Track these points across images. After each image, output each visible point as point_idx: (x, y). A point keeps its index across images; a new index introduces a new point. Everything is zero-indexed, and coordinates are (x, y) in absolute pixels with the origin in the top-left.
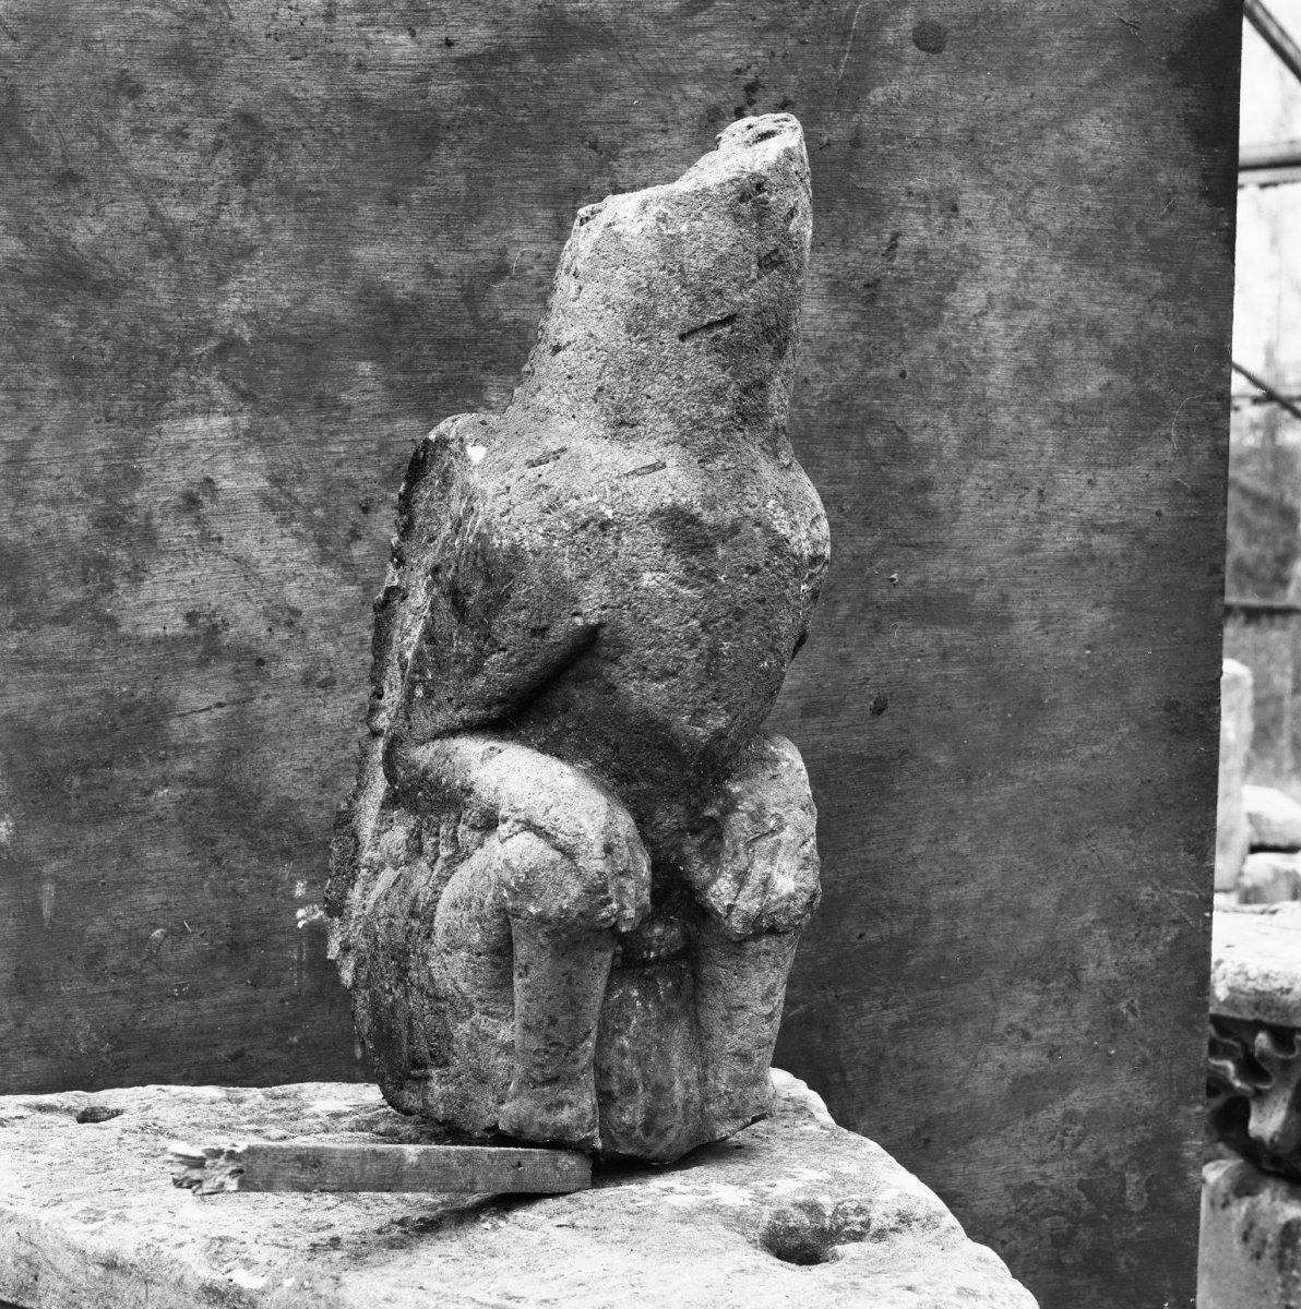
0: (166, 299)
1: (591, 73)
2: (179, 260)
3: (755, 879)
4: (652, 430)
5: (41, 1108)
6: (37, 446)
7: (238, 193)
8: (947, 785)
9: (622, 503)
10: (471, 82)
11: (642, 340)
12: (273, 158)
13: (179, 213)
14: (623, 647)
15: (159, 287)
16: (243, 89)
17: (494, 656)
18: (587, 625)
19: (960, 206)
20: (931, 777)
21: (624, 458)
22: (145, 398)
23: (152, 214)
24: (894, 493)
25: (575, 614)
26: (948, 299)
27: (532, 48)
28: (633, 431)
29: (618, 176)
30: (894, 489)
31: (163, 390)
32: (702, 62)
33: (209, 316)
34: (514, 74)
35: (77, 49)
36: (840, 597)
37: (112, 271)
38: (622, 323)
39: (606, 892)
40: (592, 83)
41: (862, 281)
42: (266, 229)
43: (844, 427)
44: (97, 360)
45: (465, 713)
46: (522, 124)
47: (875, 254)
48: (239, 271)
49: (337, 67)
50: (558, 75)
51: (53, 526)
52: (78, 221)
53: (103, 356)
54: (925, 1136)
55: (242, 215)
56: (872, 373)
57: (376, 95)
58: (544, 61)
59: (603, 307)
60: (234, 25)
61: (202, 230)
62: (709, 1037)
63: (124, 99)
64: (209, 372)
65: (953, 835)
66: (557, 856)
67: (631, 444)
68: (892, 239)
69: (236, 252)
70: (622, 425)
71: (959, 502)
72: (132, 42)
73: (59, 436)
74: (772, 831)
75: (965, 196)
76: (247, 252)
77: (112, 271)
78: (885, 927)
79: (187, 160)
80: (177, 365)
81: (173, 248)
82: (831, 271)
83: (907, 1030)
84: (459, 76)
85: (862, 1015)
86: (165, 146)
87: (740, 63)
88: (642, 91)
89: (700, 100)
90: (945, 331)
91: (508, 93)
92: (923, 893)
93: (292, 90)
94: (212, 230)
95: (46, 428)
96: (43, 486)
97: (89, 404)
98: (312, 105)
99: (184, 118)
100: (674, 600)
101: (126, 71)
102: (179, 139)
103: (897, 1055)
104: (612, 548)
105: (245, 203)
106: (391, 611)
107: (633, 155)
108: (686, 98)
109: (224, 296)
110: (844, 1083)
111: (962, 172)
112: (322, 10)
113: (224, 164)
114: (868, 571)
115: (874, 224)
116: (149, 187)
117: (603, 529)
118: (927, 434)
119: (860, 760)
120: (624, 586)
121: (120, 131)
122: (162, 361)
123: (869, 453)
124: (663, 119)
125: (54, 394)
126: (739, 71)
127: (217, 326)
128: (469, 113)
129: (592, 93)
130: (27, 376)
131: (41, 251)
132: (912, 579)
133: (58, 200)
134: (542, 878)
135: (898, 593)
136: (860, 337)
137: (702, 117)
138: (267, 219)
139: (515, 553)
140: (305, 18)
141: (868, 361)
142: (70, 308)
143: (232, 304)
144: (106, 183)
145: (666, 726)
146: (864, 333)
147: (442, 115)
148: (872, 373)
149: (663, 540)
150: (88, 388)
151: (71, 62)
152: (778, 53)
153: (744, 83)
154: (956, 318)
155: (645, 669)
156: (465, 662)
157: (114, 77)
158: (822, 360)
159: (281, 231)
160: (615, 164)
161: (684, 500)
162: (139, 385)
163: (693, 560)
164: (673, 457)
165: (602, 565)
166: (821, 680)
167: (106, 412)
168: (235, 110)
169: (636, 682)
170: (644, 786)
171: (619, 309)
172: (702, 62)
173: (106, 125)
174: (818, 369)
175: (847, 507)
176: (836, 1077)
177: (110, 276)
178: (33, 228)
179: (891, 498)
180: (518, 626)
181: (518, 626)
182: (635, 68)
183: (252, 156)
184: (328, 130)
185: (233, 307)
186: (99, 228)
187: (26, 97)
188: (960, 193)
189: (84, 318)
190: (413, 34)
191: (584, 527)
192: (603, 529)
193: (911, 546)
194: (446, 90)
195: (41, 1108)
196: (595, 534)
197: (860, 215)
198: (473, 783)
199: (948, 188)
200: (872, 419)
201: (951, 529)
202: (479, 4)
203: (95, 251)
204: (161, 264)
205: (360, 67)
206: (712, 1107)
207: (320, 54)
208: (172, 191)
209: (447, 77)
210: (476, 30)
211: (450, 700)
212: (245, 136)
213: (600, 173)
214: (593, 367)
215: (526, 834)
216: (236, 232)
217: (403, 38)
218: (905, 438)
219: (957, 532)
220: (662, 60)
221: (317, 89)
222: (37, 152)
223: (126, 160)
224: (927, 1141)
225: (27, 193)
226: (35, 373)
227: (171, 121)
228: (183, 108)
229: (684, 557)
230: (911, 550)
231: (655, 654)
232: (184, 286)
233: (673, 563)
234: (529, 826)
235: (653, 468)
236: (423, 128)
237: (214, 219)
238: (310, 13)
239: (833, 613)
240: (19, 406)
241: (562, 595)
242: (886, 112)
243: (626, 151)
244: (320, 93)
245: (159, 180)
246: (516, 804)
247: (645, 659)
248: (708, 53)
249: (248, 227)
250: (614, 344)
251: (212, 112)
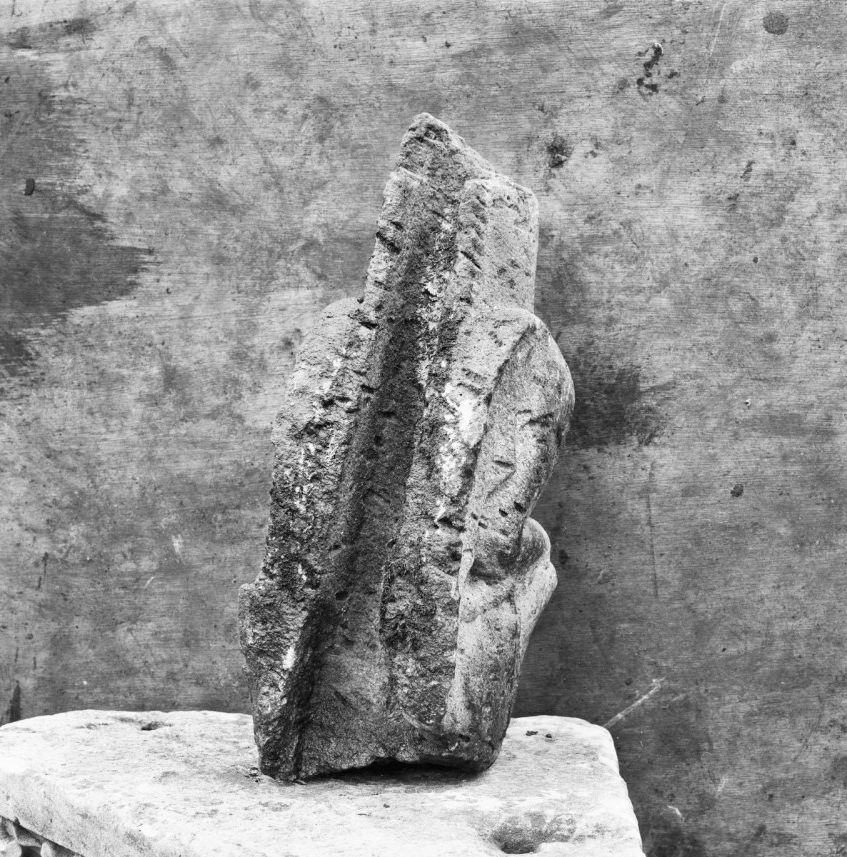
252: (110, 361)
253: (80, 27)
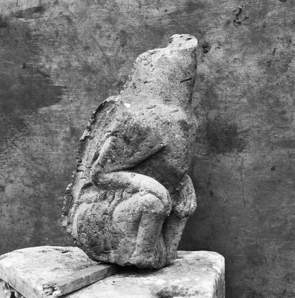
0: (107, 73)
1: (199, 15)
2: (109, 65)
3: (188, 204)
4: (174, 102)
5: (56, 249)
6: (82, 107)
7: (121, 49)
8: (291, 189)
9: (171, 119)
10: (171, 19)
11: (172, 82)
12: (128, 40)
13: (109, 54)
14: (169, 151)
15: (106, 71)
16: (122, 25)
17: (137, 152)
18: (164, 146)
19: (292, 41)
20: (287, 186)
21: (171, 108)
22: (103, 96)
23: (104, 55)
24: (276, 114)
25: (161, 143)
26: (289, 64)
27: (185, 10)
28: (169, 102)
29: (206, 39)
30: (276, 113)
31: (107, 94)
32: (225, 10)
33: (116, 77)
34: (181, 16)
35: (88, 20)
36: (262, 141)
37: (96, 68)
38: (167, 78)
39: (169, 207)
40: (199, 17)
41: (266, 61)
42: (127, 57)
43: (263, 98)
44: (94, 88)
45: (124, 166)
46: (183, 28)
47: (270, 54)
48: (122, 66)
49: (142, 18)
50: (191, 16)
51: (85, 124)
52: (89, 57)
53: (95, 87)
54: (288, 278)
55: (122, 54)
56: (270, 84)
57: (150, 24)
58: (187, 13)
59: (162, 74)
60: (120, 11)
61: (114, 58)
62: (168, 240)
63: (98, 30)
64: (116, 89)
65: (293, 202)
66: (158, 199)
67: (169, 105)
68: (274, 50)
69: (121, 62)
70: (167, 101)
71: (293, 117)
72: (99, 17)
73: (86, 105)
74: (191, 193)
75: (293, 38)
76: (123, 62)
77: (96, 68)
78: (276, 224)
79: (111, 42)
80: (109, 88)
81: (108, 62)
82: (258, 59)
83: (282, 250)
84: (168, 18)
85: (270, 246)
86: (106, 39)
87: (234, 9)
88: (211, 18)
89: (225, 19)
90: (288, 73)
91: (180, 21)
92: (286, 216)
93: (132, 25)
94: (116, 58)
95: (83, 103)
96: (83, 116)
97: (92, 97)
98: (137, 28)
99: (110, 33)
100: (181, 141)
101: (98, 23)
102: (109, 38)
103: (280, 257)
104: (170, 129)
105: (123, 51)
106: (86, 142)
107: (209, 34)
108: (221, 19)
109: (119, 72)
110: (266, 262)
111: (292, 32)
112: (138, 6)
113: (118, 43)
114: (269, 134)
115: (269, 47)
116: (102, 49)
117: (168, 124)
118: (284, 100)
119: (268, 182)
120: (172, 137)
121: (97, 37)
122: (106, 87)
123: (269, 105)
124: (216, 24)
125: (85, 96)
126: (234, 11)
127: (117, 79)
128: (171, 27)
129: (199, 19)
130: (80, 91)
131: (82, 64)
132: (281, 136)
133: (85, 53)
134: (155, 204)
135: (277, 140)
136: (266, 75)
137: (226, 23)
138: (128, 54)
139: (148, 129)
140: (135, 8)
141: (268, 81)
142: (88, 76)
143: (120, 74)
144: (94, 49)
145: (175, 169)
146: (267, 74)
147: (165, 28)
148: (270, 84)
149: (180, 127)
150: (92, 94)
151: (87, 22)
152: (244, 6)
153: (236, 14)
154: (291, 69)
155: (173, 156)
156: (128, 154)
157: (96, 25)
158: (257, 81)
159: (131, 57)
160: (205, 36)
161: (185, 118)
162: (102, 93)
163: (185, 132)
164: (180, 109)
165: (168, 132)
166: (258, 161)
167: (95, 99)
168: (120, 30)
169: (170, 159)
170: (167, 183)
171: (167, 75)
172: (225, 10)
173: (94, 36)
174: (256, 84)
175: (264, 118)
176: (264, 261)
177: (96, 69)
178: (80, 59)
179: (275, 116)
180: (146, 146)
181: (146, 146)
182: (209, 12)
183: (124, 40)
184: (140, 33)
185: (121, 75)
186: (93, 58)
187: (78, 31)
188: (292, 37)
189: (91, 78)
190: (158, 9)
191: (164, 123)
192: (168, 124)
193: (281, 128)
194: (165, 22)
195: (56, 249)
196: (167, 125)
197: (266, 44)
198: (130, 182)
199: (288, 36)
200: (270, 96)
201: (291, 124)
202: (173, 1)
203: (92, 63)
204: (106, 66)
205: (147, 18)
206: (169, 256)
207: (138, 16)
208: (108, 49)
209: (166, 19)
210: (172, 7)
211: (121, 163)
212: (123, 36)
213: (201, 39)
214: (160, 87)
215: (149, 194)
216: (121, 58)
217: (156, 10)
218: (278, 100)
219: (293, 124)
220: (215, 10)
221: (137, 24)
222: (81, 43)
223: (98, 43)
224: (288, 279)
225: (79, 52)
226: (81, 91)
227: (107, 34)
228: (110, 31)
229: (184, 131)
230: (281, 129)
231: (176, 153)
232: (111, 70)
233: (182, 133)
234: (150, 192)
235: (176, 111)
236: (161, 31)
237: (116, 55)
238: (136, 7)
239: (261, 145)
240: (78, 98)
241: (159, 139)
242: (272, 18)
243: (208, 33)
244: (138, 25)
245: (105, 47)
246: (146, 187)
247: (174, 154)
248: (227, 7)
249: (123, 56)
250: (165, 82)
251: (115, 31)
252: (52, 126)
253: (40, 9)
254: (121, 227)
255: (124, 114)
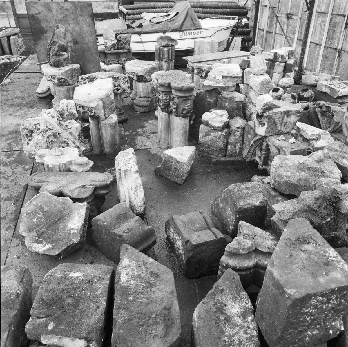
252: (47, 38)
253: (40, 13)
254: (62, 61)
255: (147, 260)
